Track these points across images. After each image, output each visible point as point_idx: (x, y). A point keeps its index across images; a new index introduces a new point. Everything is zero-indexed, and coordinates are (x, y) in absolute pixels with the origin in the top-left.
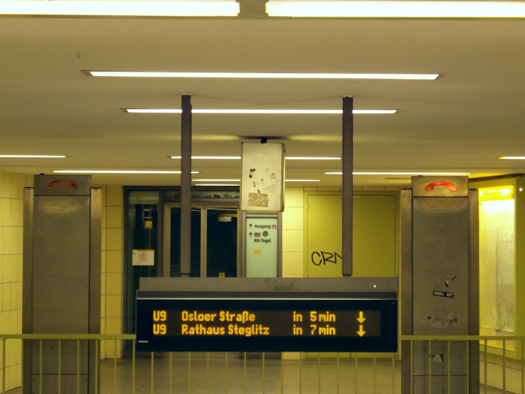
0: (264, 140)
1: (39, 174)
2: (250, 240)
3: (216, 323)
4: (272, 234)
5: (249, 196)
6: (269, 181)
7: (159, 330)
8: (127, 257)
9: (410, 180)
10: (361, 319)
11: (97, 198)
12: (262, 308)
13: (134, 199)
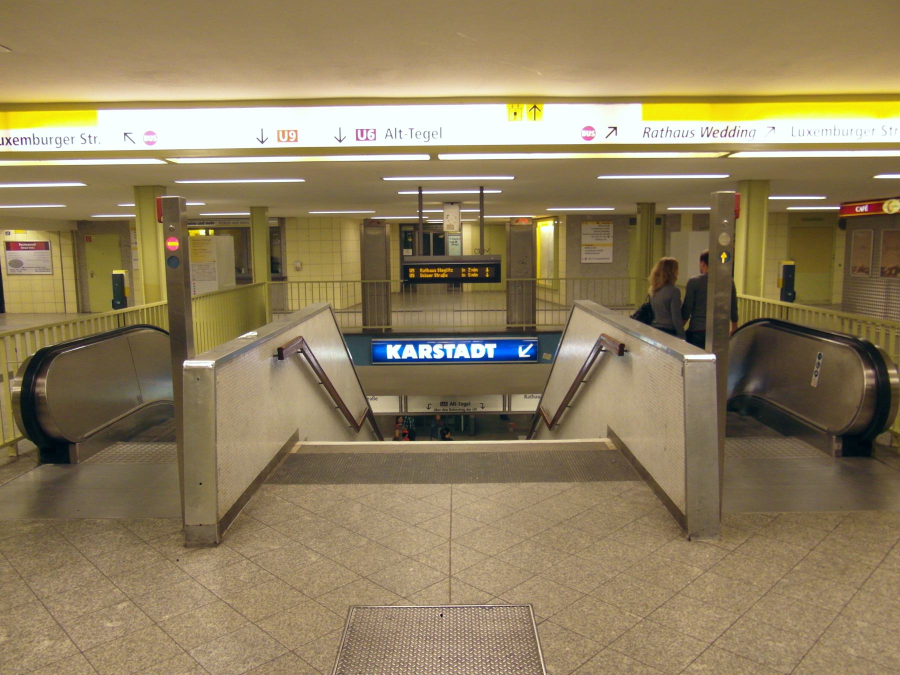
0: (452, 203)
2: (450, 244)
4: (459, 242)
6: (454, 220)
7: (412, 276)
8: (401, 252)
10: (487, 270)
11: (388, 228)
13: (403, 229)
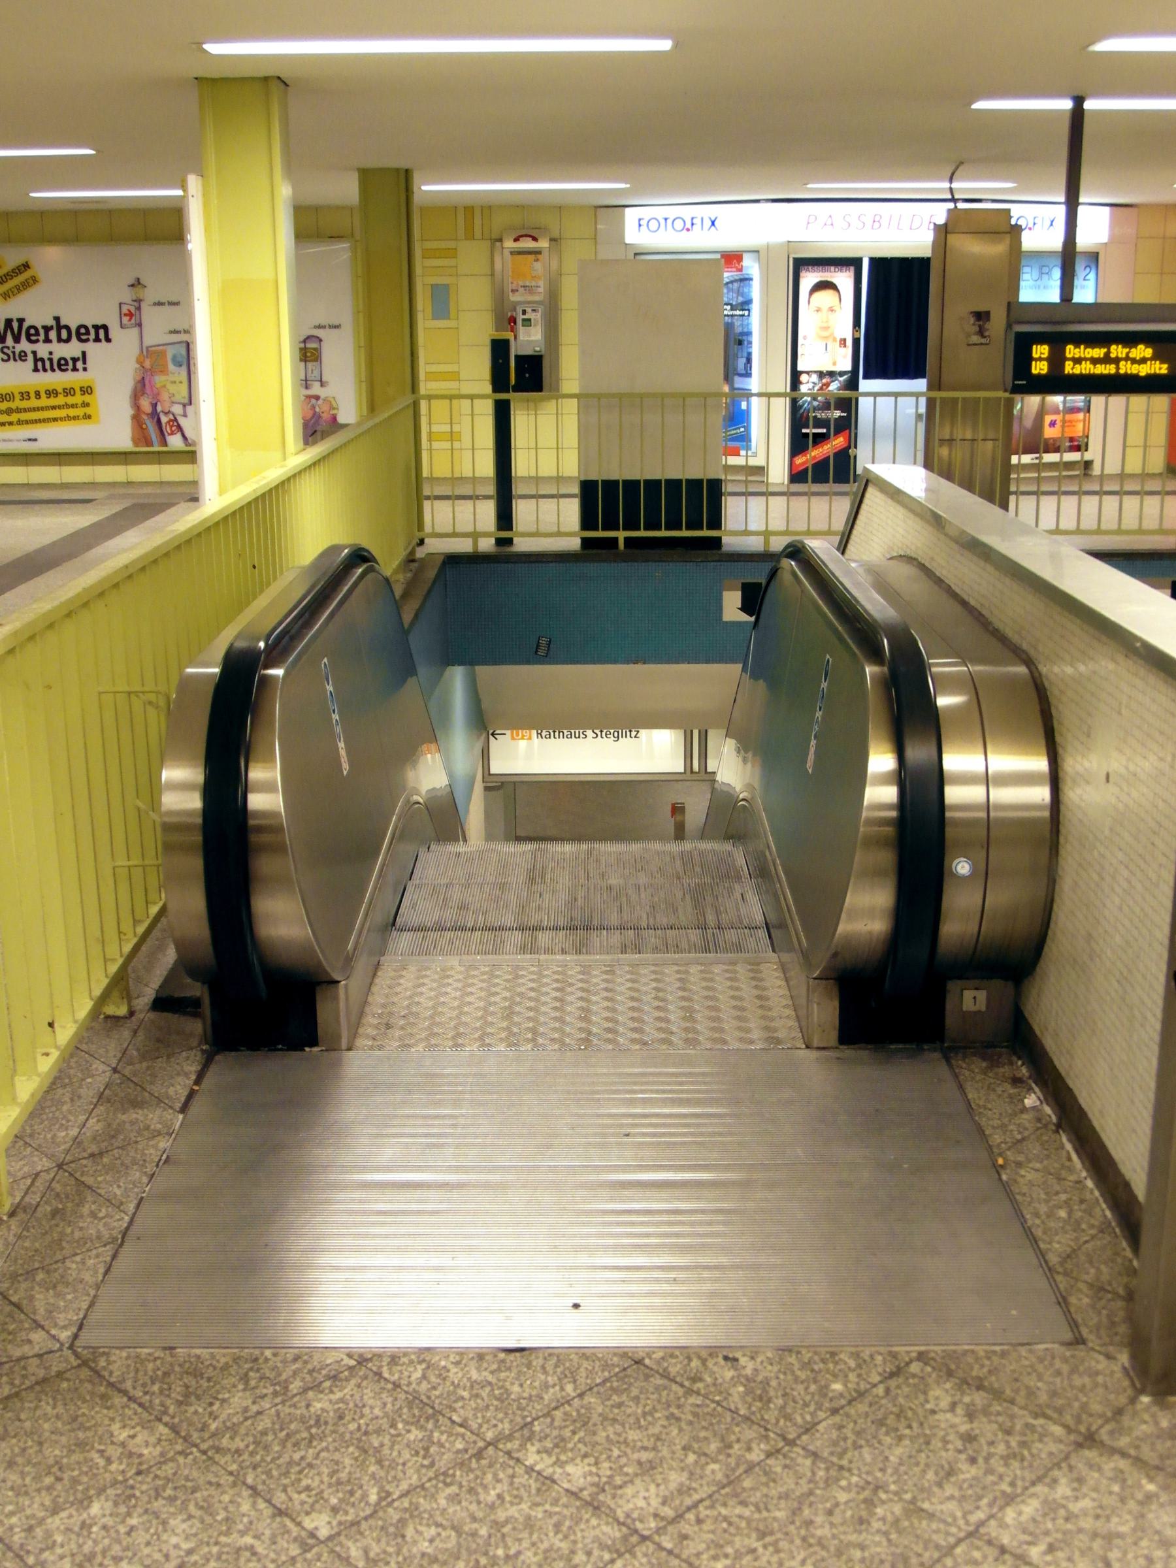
3: (1107, 360)
7: (1040, 368)
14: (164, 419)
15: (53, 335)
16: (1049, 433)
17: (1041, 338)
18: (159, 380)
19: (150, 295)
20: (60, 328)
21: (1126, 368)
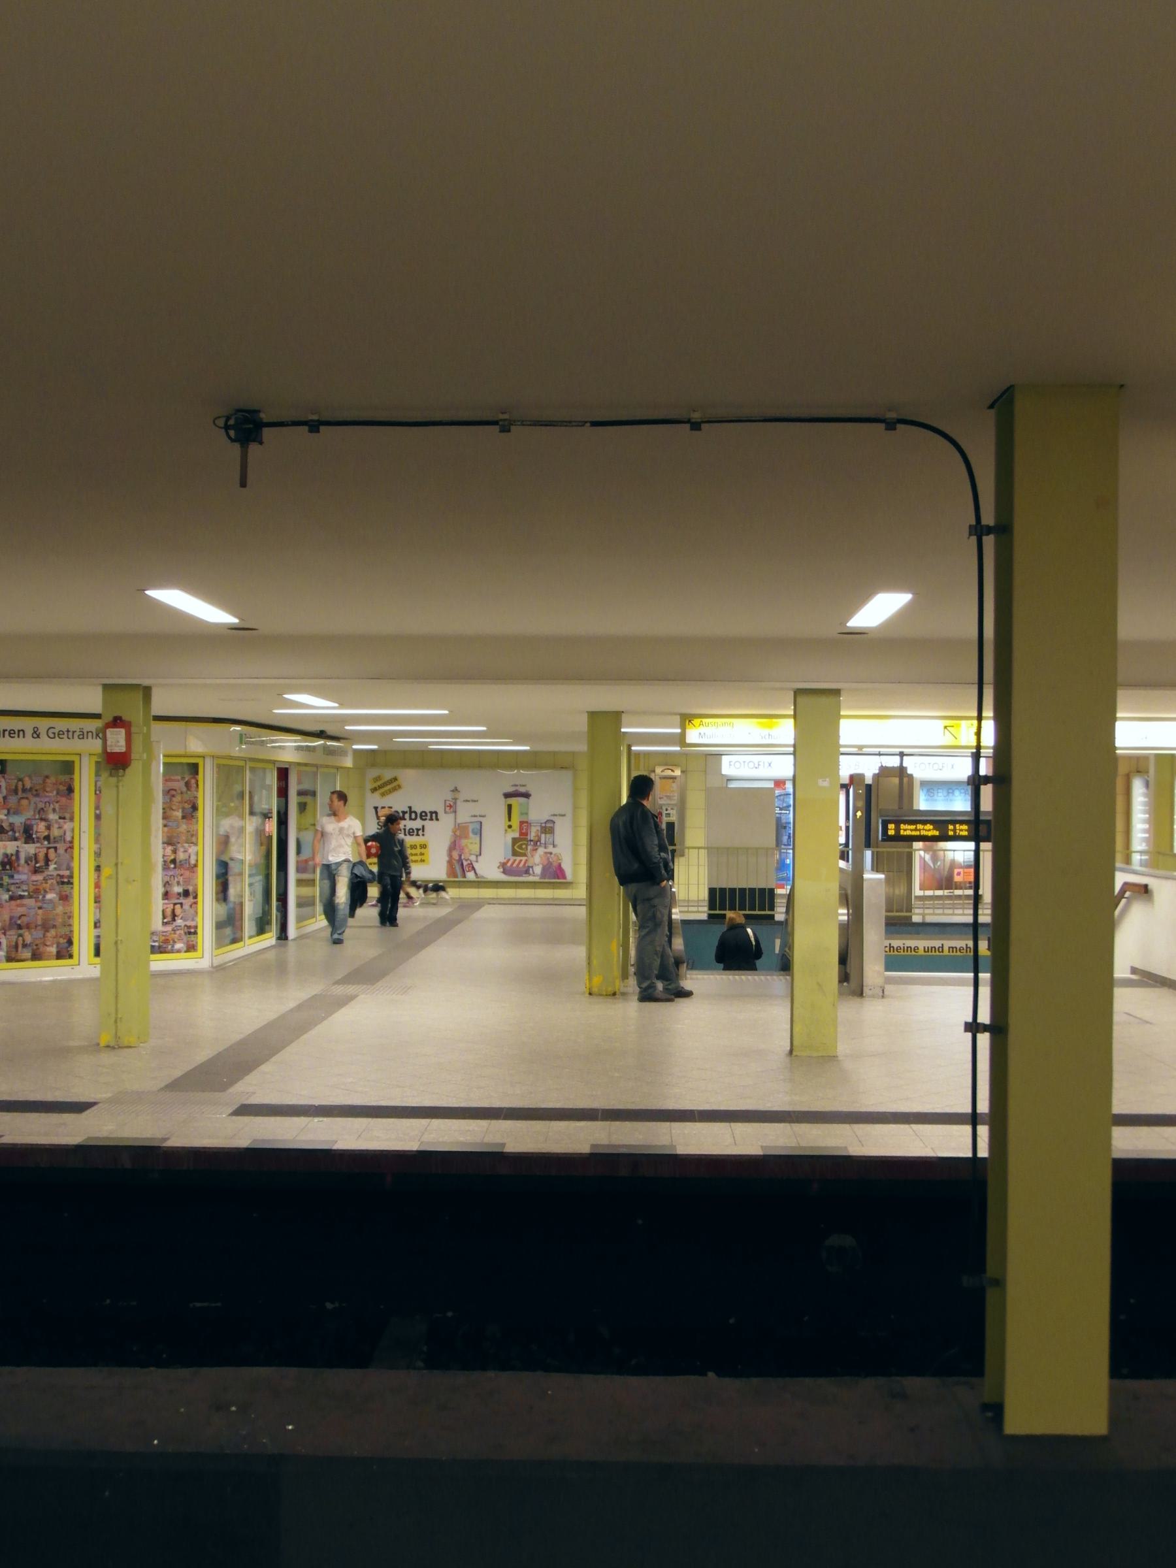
1: (909, 772)
3: (916, 830)
5: (509, 431)
7: (891, 833)
9: (979, 1036)
12: (936, 824)
14: (465, 863)
15: (407, 816)
16: (957, 879)
17: (890, 822)
18: (464, 842)
19: (462, 796)
20: (411, 812)
21: (923, 833)
